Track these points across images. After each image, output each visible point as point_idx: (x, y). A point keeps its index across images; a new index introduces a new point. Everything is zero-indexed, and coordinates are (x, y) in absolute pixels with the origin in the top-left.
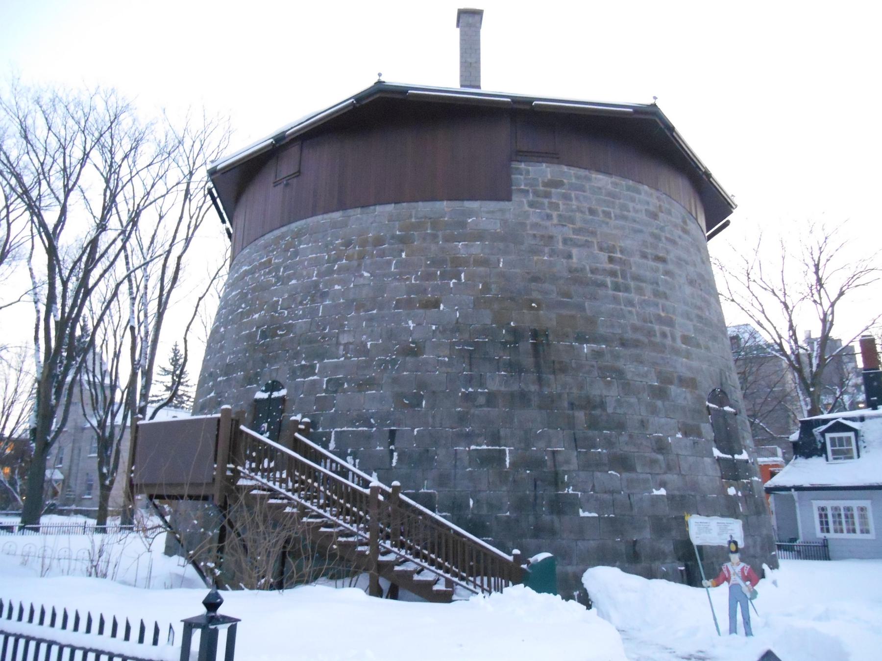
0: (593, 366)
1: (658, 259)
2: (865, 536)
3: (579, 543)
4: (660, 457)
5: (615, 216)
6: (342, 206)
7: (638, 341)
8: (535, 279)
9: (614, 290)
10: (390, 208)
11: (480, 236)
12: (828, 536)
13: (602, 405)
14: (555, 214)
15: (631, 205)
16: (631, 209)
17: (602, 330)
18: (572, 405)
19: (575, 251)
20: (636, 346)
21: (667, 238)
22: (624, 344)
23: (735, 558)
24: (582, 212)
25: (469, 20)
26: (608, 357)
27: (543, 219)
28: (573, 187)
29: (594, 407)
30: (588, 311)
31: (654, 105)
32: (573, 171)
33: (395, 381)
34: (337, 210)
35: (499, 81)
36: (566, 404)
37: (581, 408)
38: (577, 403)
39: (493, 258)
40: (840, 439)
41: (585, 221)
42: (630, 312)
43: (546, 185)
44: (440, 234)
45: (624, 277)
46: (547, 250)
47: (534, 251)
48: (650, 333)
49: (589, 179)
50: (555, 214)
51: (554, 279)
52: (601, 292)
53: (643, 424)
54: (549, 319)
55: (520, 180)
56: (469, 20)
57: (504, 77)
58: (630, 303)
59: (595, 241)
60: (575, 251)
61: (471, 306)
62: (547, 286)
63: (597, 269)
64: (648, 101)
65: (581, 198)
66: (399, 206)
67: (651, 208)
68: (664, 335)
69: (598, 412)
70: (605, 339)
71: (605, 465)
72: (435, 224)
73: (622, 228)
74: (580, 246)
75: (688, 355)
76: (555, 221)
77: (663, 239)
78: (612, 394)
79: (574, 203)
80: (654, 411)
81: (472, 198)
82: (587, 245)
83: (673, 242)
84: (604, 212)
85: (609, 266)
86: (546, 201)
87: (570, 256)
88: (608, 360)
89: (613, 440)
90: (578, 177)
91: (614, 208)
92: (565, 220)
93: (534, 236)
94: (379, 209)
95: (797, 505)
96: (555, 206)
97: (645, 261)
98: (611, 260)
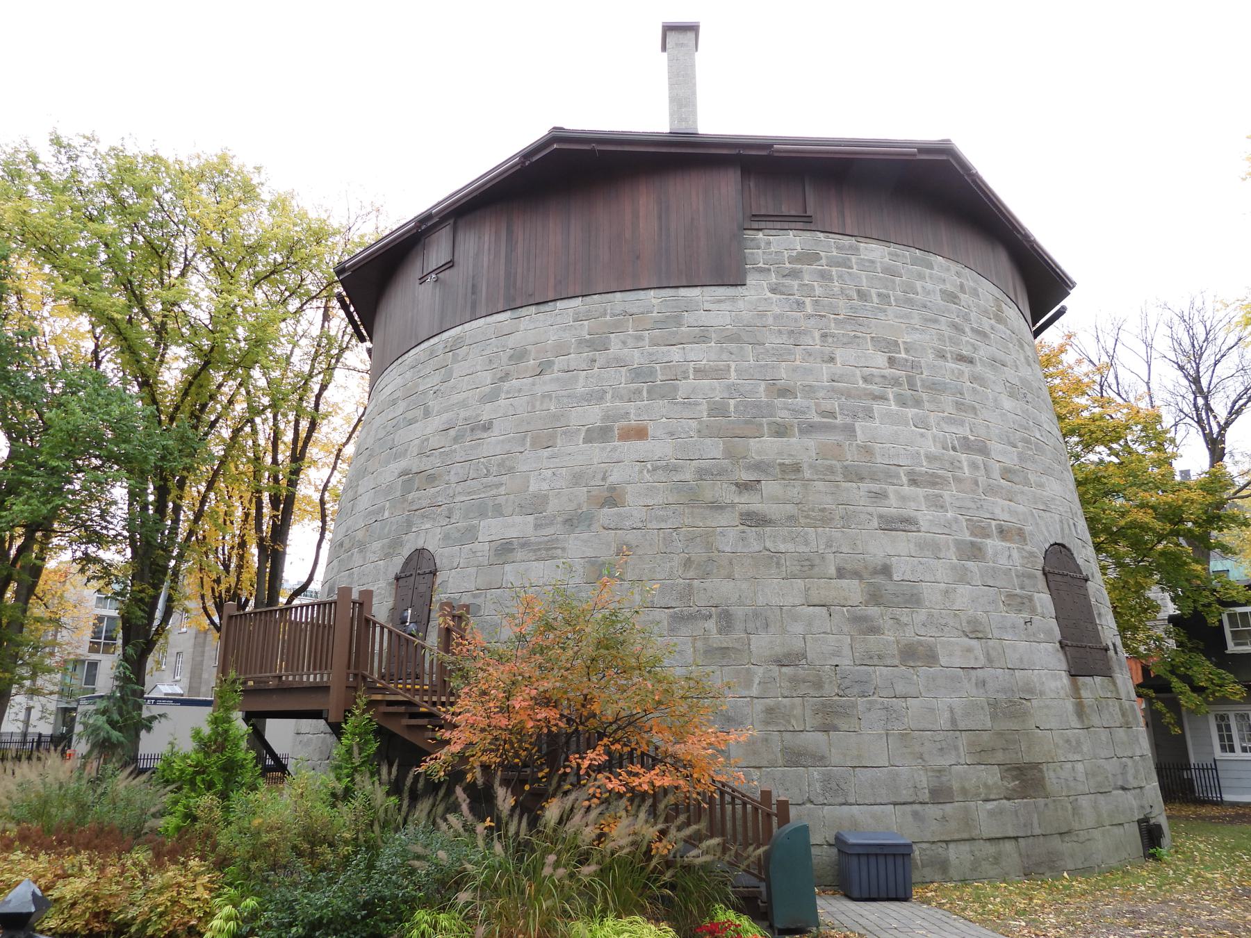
8: (785, 392)
13: (886, 570)
14: (807, 300)
15: (919, 284)
16: (919, 290)
20: (934, 484)
26: (893, 500)
28: (833, 263)
32: (833, 240)
48: (954, 465)
50: (807, 300)
51: (809, 390)
52: (877, 407)
65: (846, 277)
67: (949, 287)
76: (809, 310)
85: (889, 372)
86: (795, 283)
88: (892, 508)
89: (904, 619)
91: (894, 289)
97: (941, 362)
98: (891, 361)
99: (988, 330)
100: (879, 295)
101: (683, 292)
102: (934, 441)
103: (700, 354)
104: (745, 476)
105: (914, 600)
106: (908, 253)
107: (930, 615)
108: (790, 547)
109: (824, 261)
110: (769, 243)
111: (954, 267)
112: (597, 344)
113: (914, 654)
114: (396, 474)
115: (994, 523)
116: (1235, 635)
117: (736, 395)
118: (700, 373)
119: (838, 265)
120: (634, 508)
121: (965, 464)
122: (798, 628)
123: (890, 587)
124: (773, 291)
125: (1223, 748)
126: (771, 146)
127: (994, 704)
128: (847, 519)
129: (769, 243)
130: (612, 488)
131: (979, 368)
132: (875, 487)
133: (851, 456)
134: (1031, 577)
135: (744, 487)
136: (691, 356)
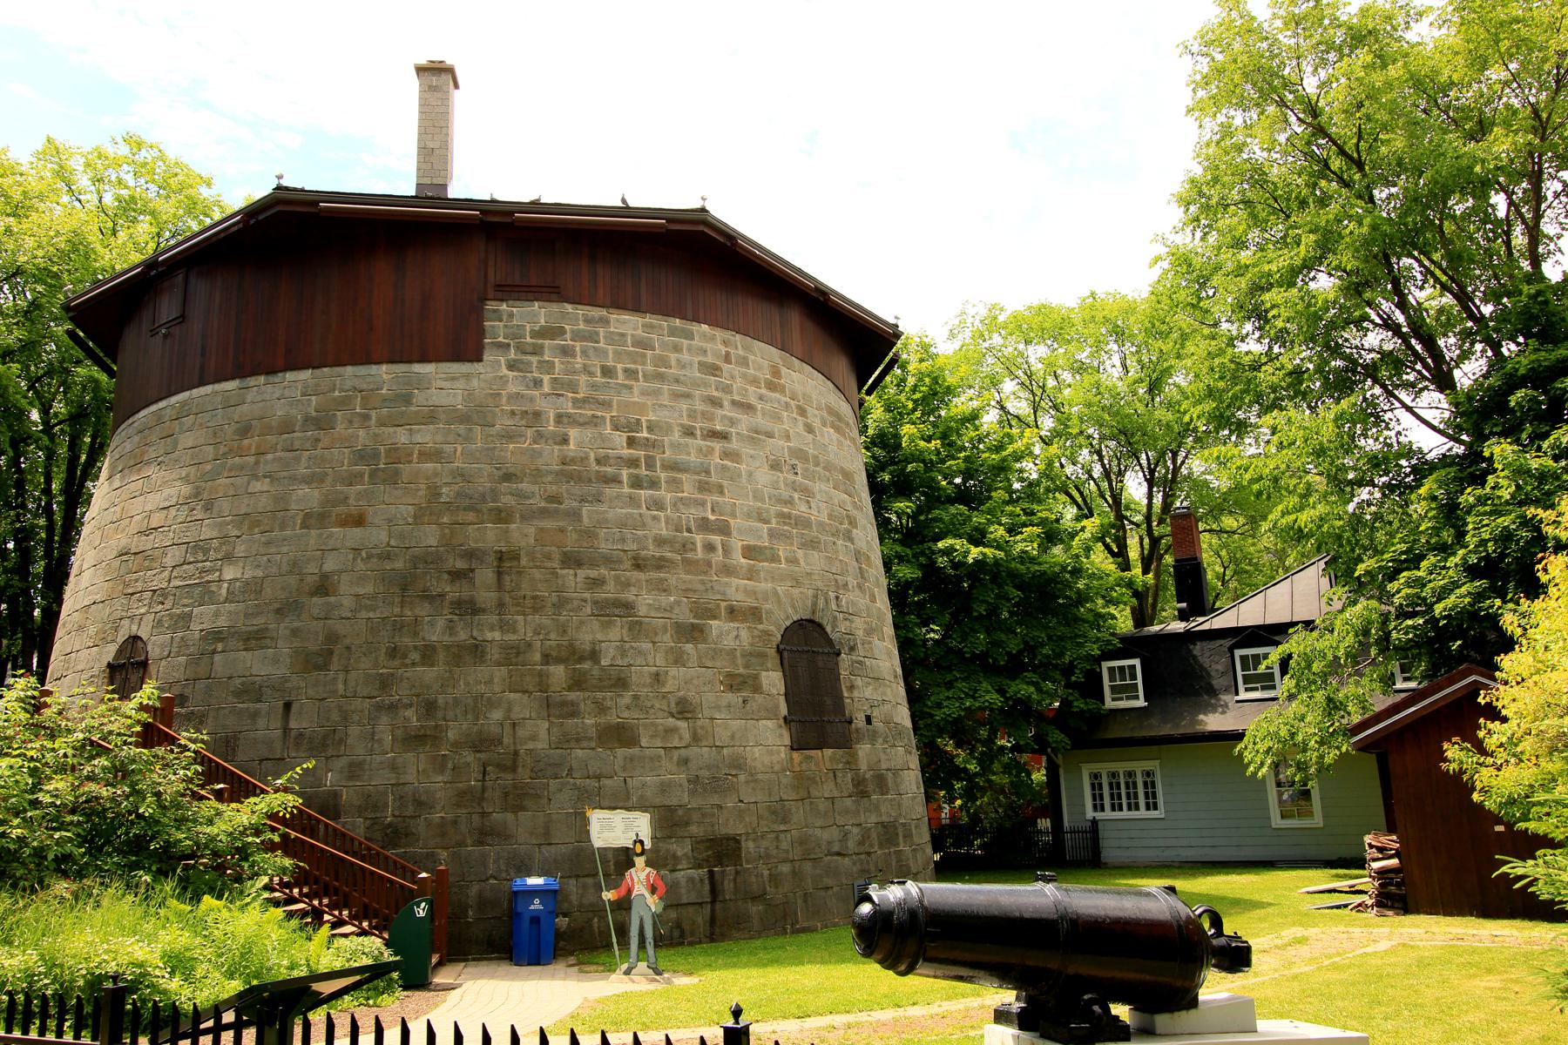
0: (585, 601)
1: (714, 435)
2: (1153, 814)
3: (544, 849)
4: (683, 724)
5: (644, 376)
6: (241, 372)
7: (662, 559)
8: (508, 477)
9: (632, 486)
10: (305, 375)
11: (431, 417)
12: (1099, 815)
13: (594, 655)
14: (546, 378)
15: (673, 357)
16: (673, 363)
17: (604, 547)
18: (547, 659)
19: (573, 433)
20: (659, 568)
21: (734, 403)
22: (638, 564)
23: (640, 861)
24: (591, 374)
25: (437, 76)
26: (611, 586)
27: (528, 387)
28: (578, 336)
29: (581, 659)
30: (586, 520)
31: (703, 210)
32: (581, 311)
33: (295, 632)
34: (233, 379)
35: (471, 181)
36: (537, 657)
37: (559, 660)
38: (554, 654)
39: (448, 448)
40: (1122, 668)
41: (594, 386)
42: (655, 518)
43: (534, 334)
44: (373, 413)
45: (650, 465)
46: (529, 432)
47: (510, 436)
48: (686, 546)
49: (605, 322)
50: (546, 378)
51: (537, 475)
52: (610, 491)
53: (657, 678)
54: (522, 534)
55: (496, 329)
56: (437, 76)
57: (494, 168)
58: (658, 505)
59: (608, 416)
60: (573, 433)
61: (410, 520)
62: (525, 486)
63: (607, 457)
64: (697, 205)
65: (591, 353)
66: (317, 372)
67: (710, 359)
68: (710, 548)
69: (586, 666)
70: (609, 561)
71: (591, 739)
72: (368, 396)
73: (657, 393)
74: (581, 425)
75: (751, 575)
76: (546, 389)
77: (726, 403)
78: (609, 639)
79: (579, 361)
80: (679, 660)
81: (424, 359)
82: (594, 422)
83: (748, 408)
84: (626, 370)
85: (626, 452)
86: (534, 359)
87: (565, 441)
88: (610, 592)
89: (609, 703)
90: (587, 321)
91: (644, 364)
92: (562, 386)
93: (513, 413)
94: (290, 376)
95: (1061, 771)
96: (548, 367)
97: (689, 440)
98: (631, 442)
99: (753, 400)
100: (626, 370)
101: (418, 368)
102: (667, 523)
103: (425, 436)
104: (461, 564)
105: (621, 683)
106: (664, 323)
107: (636, 697)
108: (497, 635)
109: (568, 336)
110: (511, 315)
111: (719, 334)
112: (322, 422)
113: (621, 735)
114: (115, 553)
115: (723, 604)
116: (1114, 689)
117: (459, 479)
118: (426, 456)
119: (583, 339)
120: (345, 596)
121: (699, 545)
122: (497, 715)
123: (596, 672)
124: (511, 367)
125: (1095, 808)
126: (513, 213)
127: (695, 780)
128: (560, 604)
129: (511, 315)
130: (325, 577)
131: (734, 445)
132: (593, 573)
133: (571, 541)
134: (762, 655)
135: (456, 575)
136: (418, 438)
